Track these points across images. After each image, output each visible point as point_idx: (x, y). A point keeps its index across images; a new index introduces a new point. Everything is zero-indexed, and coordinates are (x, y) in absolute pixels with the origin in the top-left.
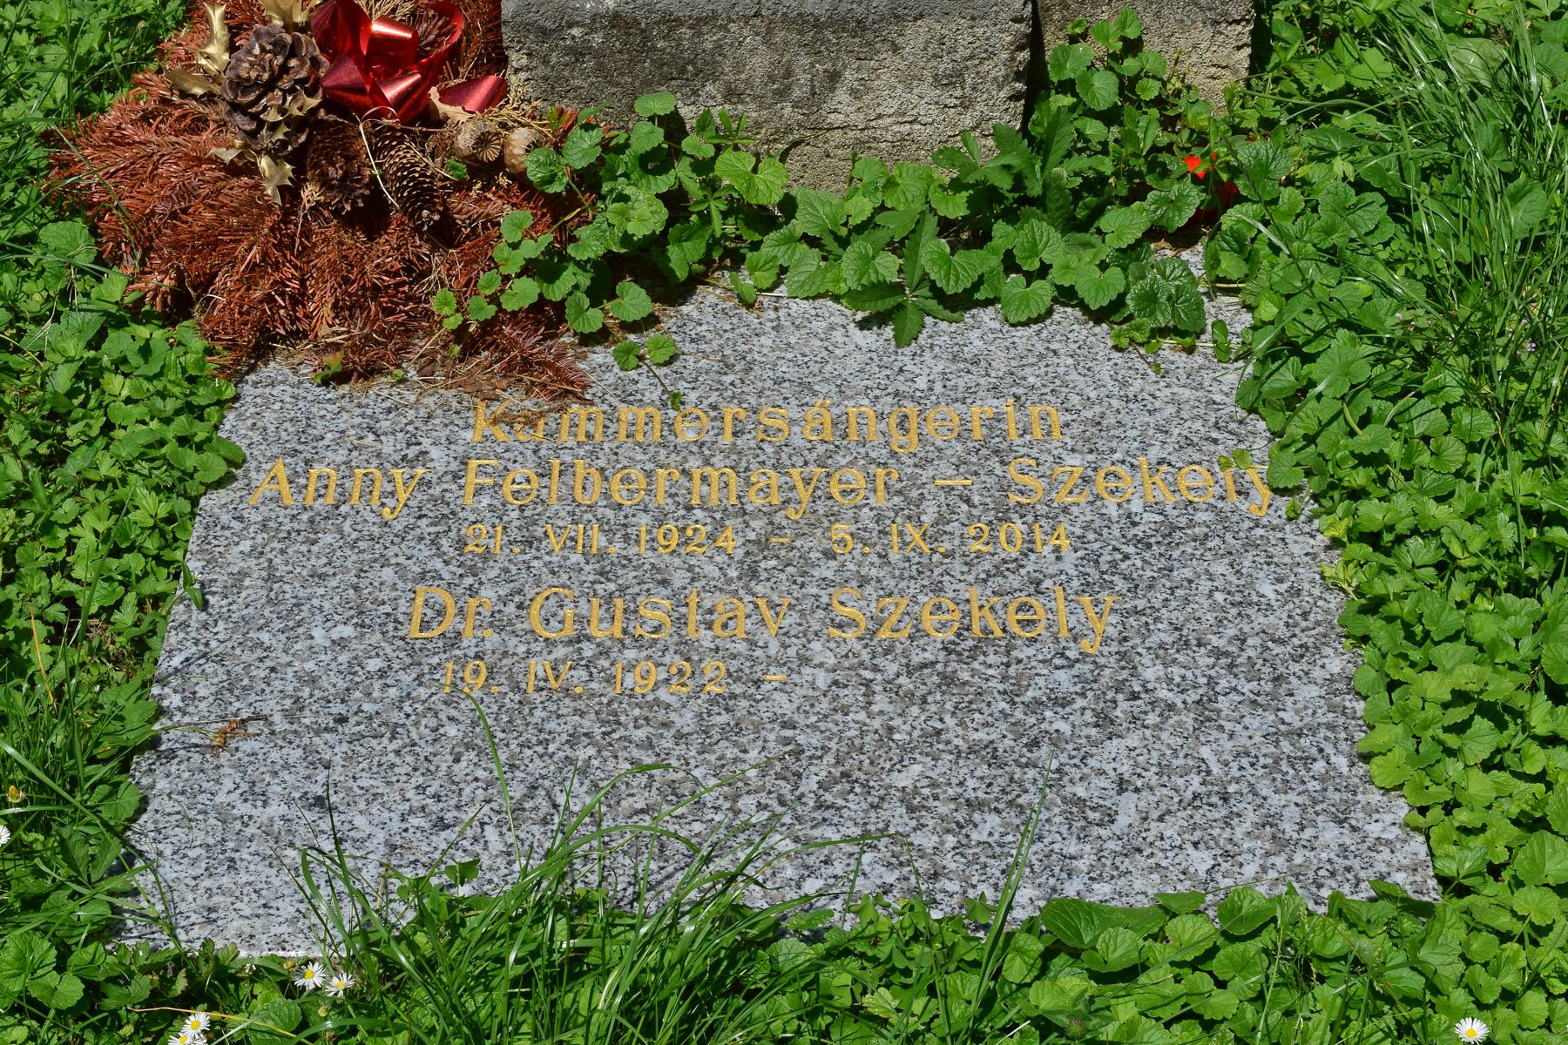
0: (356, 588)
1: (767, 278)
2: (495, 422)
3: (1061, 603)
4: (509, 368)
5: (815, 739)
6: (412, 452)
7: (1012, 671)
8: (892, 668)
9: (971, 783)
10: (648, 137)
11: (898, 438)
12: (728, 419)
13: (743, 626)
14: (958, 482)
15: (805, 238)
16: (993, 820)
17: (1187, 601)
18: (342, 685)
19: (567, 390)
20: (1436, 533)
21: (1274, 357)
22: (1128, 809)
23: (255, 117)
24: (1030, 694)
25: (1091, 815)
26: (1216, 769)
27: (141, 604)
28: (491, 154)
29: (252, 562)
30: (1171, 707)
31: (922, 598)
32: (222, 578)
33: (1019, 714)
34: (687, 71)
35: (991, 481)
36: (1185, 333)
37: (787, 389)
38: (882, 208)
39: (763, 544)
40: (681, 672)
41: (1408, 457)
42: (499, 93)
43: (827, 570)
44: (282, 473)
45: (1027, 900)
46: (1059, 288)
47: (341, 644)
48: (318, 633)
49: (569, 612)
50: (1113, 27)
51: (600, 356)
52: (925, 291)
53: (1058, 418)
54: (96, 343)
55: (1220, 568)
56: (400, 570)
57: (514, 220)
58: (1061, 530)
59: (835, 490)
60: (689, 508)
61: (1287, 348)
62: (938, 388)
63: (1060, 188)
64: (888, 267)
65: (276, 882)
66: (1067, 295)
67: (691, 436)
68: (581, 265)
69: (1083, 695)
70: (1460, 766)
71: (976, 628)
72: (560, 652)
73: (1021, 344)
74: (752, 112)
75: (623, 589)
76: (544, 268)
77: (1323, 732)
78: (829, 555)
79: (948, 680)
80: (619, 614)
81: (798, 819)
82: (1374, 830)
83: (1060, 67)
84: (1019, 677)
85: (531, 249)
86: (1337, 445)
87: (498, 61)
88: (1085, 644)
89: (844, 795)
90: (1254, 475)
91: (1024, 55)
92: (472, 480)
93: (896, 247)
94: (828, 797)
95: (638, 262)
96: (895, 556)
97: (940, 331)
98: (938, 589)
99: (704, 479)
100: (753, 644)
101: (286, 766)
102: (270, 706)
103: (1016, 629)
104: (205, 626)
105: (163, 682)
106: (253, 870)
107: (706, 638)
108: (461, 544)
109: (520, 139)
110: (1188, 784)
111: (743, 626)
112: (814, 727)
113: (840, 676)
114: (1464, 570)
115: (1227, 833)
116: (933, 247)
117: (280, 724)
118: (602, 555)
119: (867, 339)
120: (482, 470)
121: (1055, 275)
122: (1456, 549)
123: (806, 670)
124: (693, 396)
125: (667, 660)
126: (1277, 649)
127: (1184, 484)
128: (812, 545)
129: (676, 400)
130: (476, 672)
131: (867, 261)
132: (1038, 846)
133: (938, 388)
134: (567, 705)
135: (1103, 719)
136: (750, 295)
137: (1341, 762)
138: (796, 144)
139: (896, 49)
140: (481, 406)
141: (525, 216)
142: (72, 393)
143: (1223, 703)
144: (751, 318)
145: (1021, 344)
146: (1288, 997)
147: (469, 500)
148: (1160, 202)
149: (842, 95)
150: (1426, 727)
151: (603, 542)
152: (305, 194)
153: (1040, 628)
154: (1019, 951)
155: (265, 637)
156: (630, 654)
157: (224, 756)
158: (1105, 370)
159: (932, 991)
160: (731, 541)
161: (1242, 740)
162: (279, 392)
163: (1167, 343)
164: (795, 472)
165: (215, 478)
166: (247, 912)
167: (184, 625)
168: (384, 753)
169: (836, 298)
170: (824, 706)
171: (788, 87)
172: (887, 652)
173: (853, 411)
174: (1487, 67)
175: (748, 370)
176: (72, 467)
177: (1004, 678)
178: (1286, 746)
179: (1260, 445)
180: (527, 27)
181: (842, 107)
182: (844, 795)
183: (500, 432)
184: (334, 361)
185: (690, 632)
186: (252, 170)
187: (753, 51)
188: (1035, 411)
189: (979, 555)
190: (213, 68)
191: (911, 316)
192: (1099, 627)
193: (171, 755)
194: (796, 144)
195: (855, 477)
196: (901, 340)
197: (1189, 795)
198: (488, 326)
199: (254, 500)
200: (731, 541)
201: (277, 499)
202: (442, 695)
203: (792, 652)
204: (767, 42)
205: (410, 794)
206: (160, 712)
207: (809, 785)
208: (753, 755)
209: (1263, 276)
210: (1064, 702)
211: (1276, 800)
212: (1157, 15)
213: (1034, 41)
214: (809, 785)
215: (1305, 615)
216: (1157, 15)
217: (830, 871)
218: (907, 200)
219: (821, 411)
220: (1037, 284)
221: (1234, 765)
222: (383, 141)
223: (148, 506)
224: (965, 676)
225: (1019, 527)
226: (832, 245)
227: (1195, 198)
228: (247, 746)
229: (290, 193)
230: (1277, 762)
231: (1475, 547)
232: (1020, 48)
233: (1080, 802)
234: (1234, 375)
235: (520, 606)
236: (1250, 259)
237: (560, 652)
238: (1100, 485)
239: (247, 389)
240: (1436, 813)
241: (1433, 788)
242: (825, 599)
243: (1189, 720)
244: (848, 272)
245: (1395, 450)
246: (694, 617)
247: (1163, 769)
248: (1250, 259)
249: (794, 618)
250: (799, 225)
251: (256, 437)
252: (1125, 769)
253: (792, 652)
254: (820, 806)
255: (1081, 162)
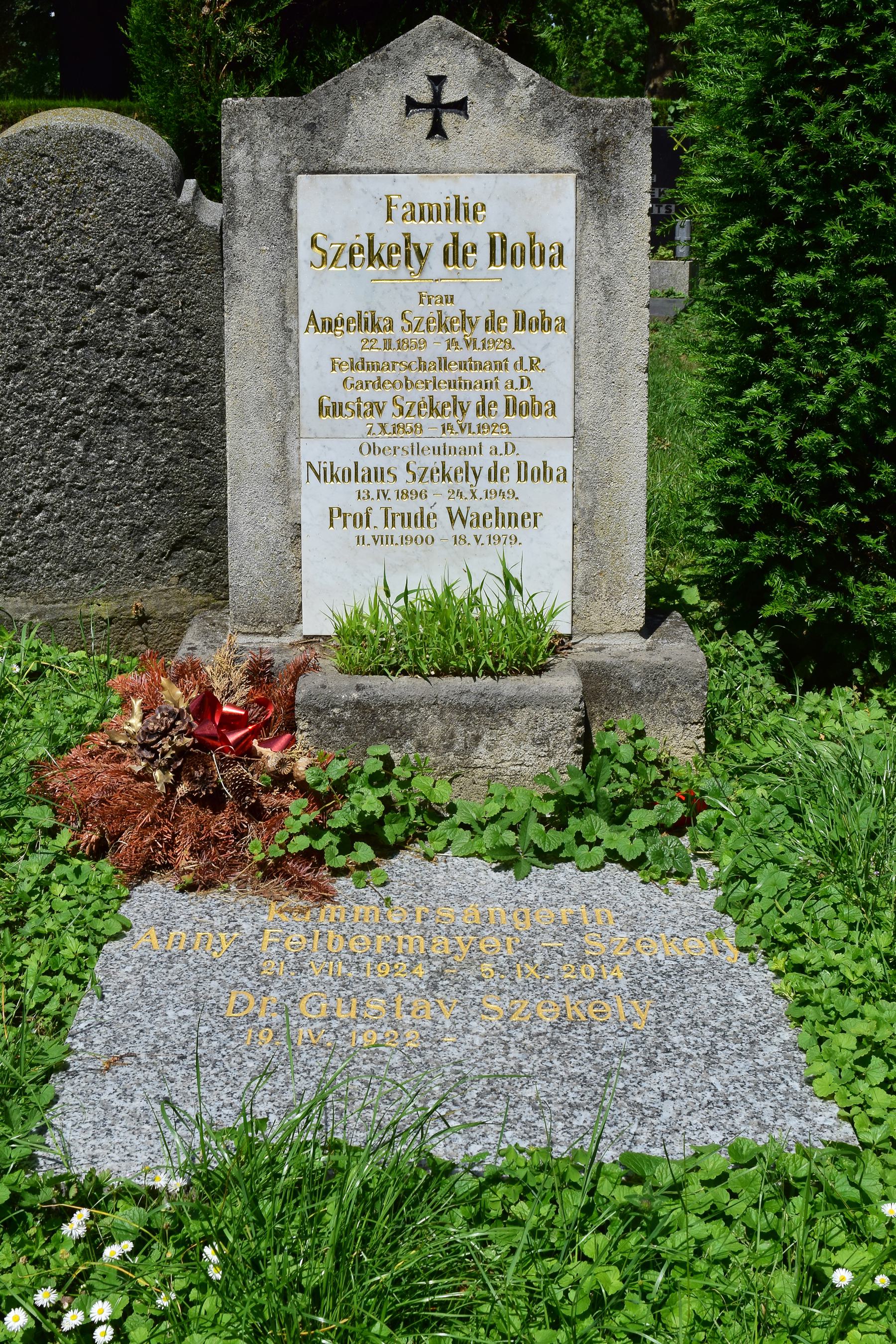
0: (195, 991)
1: (440, 846)
2: (281, 912)
3: (620, 1005)
4: (291, 884)
5: (475, 1072)
6: (231, 925)
7: (593, 1037)
8: (520, 1036)
9: (571, 1095)
10: (373, 766)
11: (518, 923)
12: (419, 913)
13: (429, 1013)
14: (555, 944)
15: (463, 826)
16: (586, 1115)
17: (694, 1003)
18: (183, 1039)
19: (325, 896)
20: (837, 968)
21: (733, 880)
22: (668, 1110)
23: (154, 751)
24: (604, 1049)
25: (646, 1112)
26: (720, 1089)
27: (62, 1001)
28: (286, 771)
29: (132, 977)
30: (690, 1056)
31: (537, 1001)
32: (113, 984)
33: (598, 1059)
34: (396, 733)
35: (574, 944)
36: (683, 876)
37: (452, 899)
38: (505, 810)
39: (441, 973)
40: (391, 1036)
41: (816, 931)
42: (293, 741)
43: (480, 986)
44: (153, 933)
45: (608, 1155)
46: (607, 850)
47: (185, 1018)
48: (171, 1014)
49: (323, 1005)
50: (628, 723)
51: (342, 881)
52: (531, 854)
53: (611, 915)
54: (50, 868)
55: (712, 987)
56: (222, 983)
57: (297, 804)
58: (617, 968)
59: (482, 947)
60: (396, 955)
61: (738, 875)
62: (541, 899)
63: (605, 798)
64: (510, 838)
65: (137, 1142)
66: (613, 856)
67: (397, 920)
68: (335, 831)
69: (636, 1050)
70: (867, 1085)
71: (570, 1015)
72: (318, 1025)
73: (588, 880)
74: (432, 757)
75: (356, 994)
76: (315, 830)
77: (782, 1070)
78: (480, 979)
79: (554, 1042)
80: (354, 1006)
81: (466, 1113)
82: (820, 1120)
83: (601, 742)
84: (597, 1041)
85: (307, 819)
86: (774, 922)
87: (291, 727)
88: (636, 1025)
89: (494, 1101)
90: (729, 943)
91: (581, 729)
92: (267, 939)
93: (513, 828)
94: (484, 1102)
95: (369, 830)
96: (519, 979)
97: (541, 874)
98: (546, 996)
99: (405, 941)
100: (435, 1022)
101: (147, 1081)
102: (139, 1049)
103: (594, 1017)
104: (102, 1008)
105: (73, 1036)
106: (121, 1135)
107: (407, 1019)
108: (259, 970)
109: (302, 763)
110: (704, 1096)
111: (429, 1013)
112: (474, 1066)
113: (489, 1039)
114: (855, 987)
115: (730, 1122)
116: (534, 830)
117: (144, 1058)
118: (344, 977)
119: (500, 876)
120: (272, 935)
121: (605, 844)
122: (849, 976)
123: (468, 1036)
124: (398, 901)
125: (383, 1029)
126: (751, 1028)
127: (687, 947)
128: (470, 974)
129: (388, 902)
130: (266, 1034)
131: (498, 835)
132: (615, 1128)
133: (541, 899)
134: (322, 1052)
135: (650, 1062)
136: (431, 854)
137: (796, 1086)
138: (457, 776)
139: (511, 724)
140: (273, 904)
141: (304, 802)
142: (32, 893)
143: (721, 1054)
144: (431, 865)
145: (588, 880)
146: (776, 1205)
147: (265, 949)
148: (662, 811)
149: (482, 749)
150: (844, 1063)
151: (345, 970)
152: (179, 790)
153: (608, 1016)
154: (607, 1175)
155: (138, 1014)
156: (361, 1027)
157: (108, 1075)
158: (637, 893)
159: (553, 1201)
160: (421, 971)
161: (734, 1073)
162: (156, 894)
163: (672, 881)
164: (459, 938)
165: (113, 933)
166: (117, 1158)
167: (89, 1008)
168: (208, 1074)
169: (480, 856)
170: (480, 1054)
171: (452, 744)
172: (516, 1027)
173: (491, 910)
174: (834, 754)
175: (430, 889)
176: (28, 929)
177: (588, 1041)
178: (761, 1077)
179: (730, 929)
180: (309, 707)
181: (482, 755)
182: (494, 1101)
183: (284, 917)
184: (187, 879)
185: (397, 1016)
186: (150, 778)
187: (433, 723)
188: (598, 911)
189: (569, 980)
190: (132, 730)
191: (524, 867)
192: (643, 1016)
193: (75, 1073)
194: (457, 776)
195: (495, 941)
196: (518, 877)
197: (705, 1102)
198: (279, 861)
199: (137, 945)
200: (421, 971)
201: (149, 947)
202: (245, 1046)
203: (459, 1027)
204: (441, 718)
205: (223, 1097)
206: (69, 1051)
207: (472, 1095)
208: (437, 1080)
209: (722, 847)
210: (625, 1053)
211: (758, 1105)
212: (653, 718)
213: (585, 722)
214: (472, 1095)
215: (765, 1011)
216: (653, 718)
217: (486, 1140)
218: (519, 805)
219: (473, 909)
220: (595, 849)
221: (731, 1087)
222: (225, 764)
223: (73, 946)
224: (565, 1040)
225: (592, 967)
226: (477, 828)
227: (681, 809)
228: (123, 1070)
229: (171, 788)
230: (757, 1085)
231: (860, 973)
232: (579, 725)
233: (639, 1105)
234: (711, 896)
235: (294, 1001)
236: (714, 838)
237: (318, 1025)
238: (639, 946)
239: (136, 894)
240: (855, 1110)
241: (852, 1098)
242: (478, 1001)
243: (702, 1063)
244: (487, 838)
245: (807, 926)
246: (399, 1008)
247: (687, 1088)
248: (714, 838)
249: (459, 1009)
250: (458, 818)
251: (139, 916)
252: (665, 1088)
253: (459, 1027)
254: (478, 1105)
255: (615, 785)
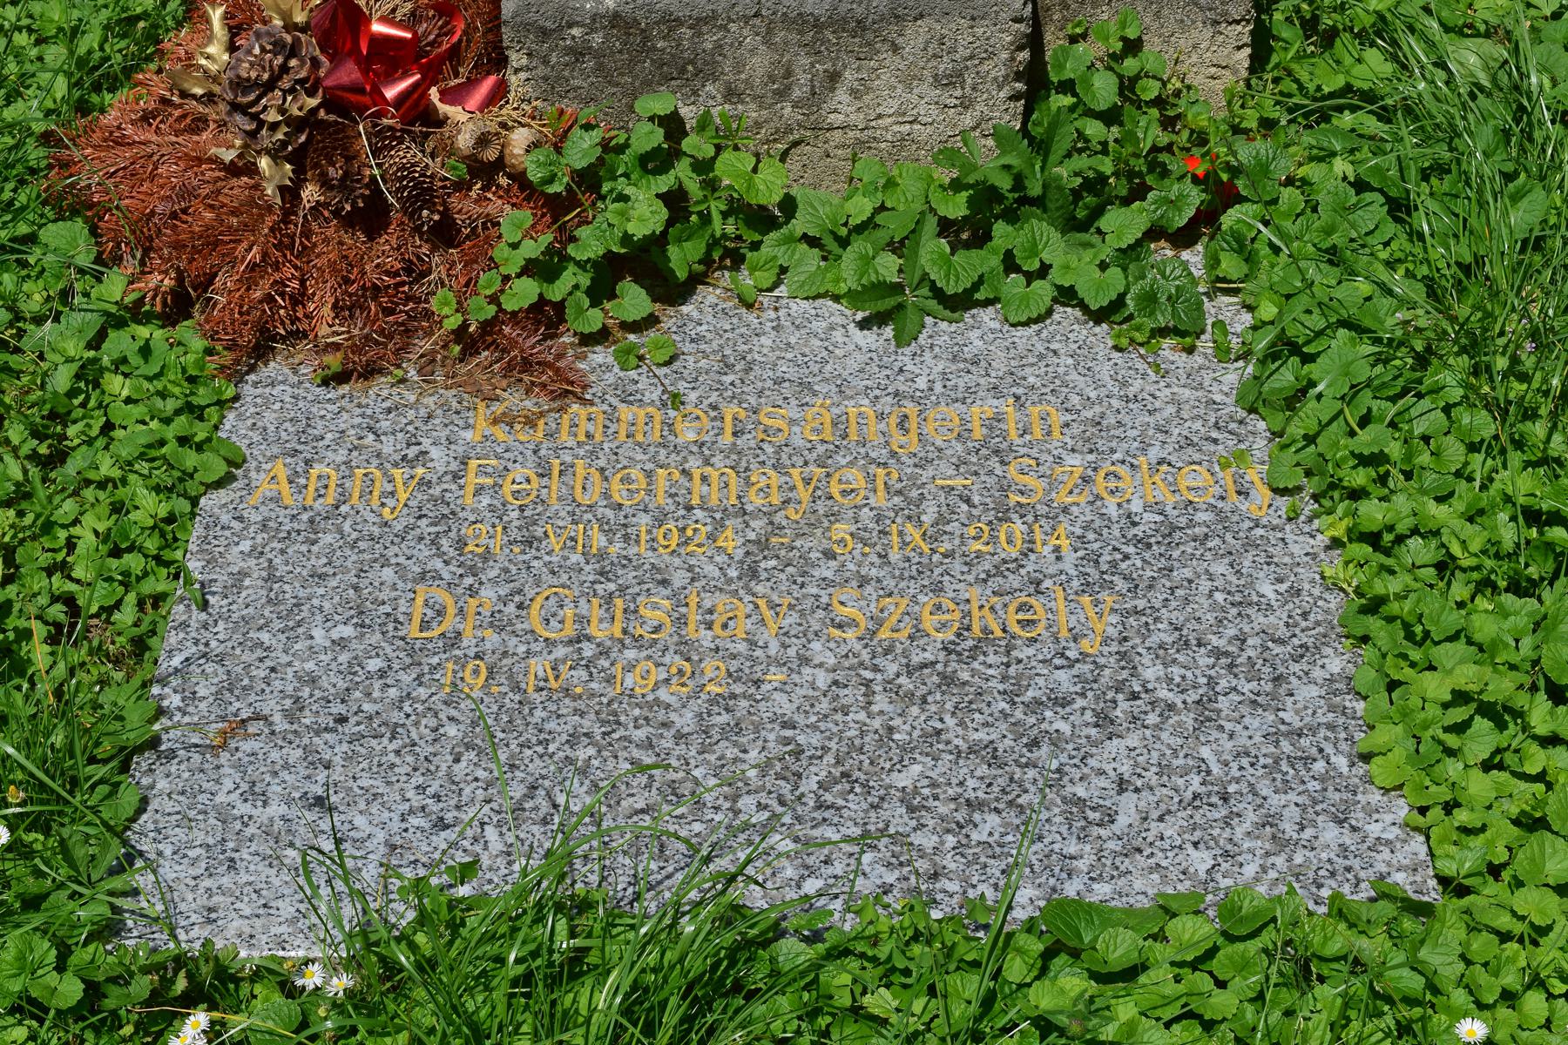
0: (356, 588)
1: (767, 278)
2: (495, 422)
3: (1061, 603)
4: (509, 368)
5: (815, 739)
6: (412, 452)
7: (1012, 671)
8: (892, 668)
9: (971, 783)
10: (648, 137)
11: (898, 438)
12: (728, 419)
13: (743, 626)
14: (958, 482)
15: (805, 238)
16: (993, 820)
17: (1187, 601)
18: (342, 685)
19: (567, 390)
20: (1436, 533)
21: (1274, 357)
22: (1128, 809)
23: (255, 117)
24: (1030, 694)
25: (1091, 815)
26: (1216, 769)
27: (141, 604)
28: (491, 154)
29: (252, 562)
30: (1171, 707)
31: (922, 598)
32: (222, 578)
33: (1019, 714)
34: (687, 71)
35: (991, 481)
36: (1185, 333)
37: (787, 389)
38: (882, 208)
39: (763, 544)
40: (681, 672)
41: (1408, 457)
42: (499, 93)
43: (827, 570)
44: (282, 473)
45: (1027, 900)
46: (1059, 288)
47: (341, 644)
48: (318, 633)
49: (569, 612)
50: (1113, 27)
51: (600, 356)
52: (925, 291)
53: (1058, 418)
54: (96, 343)
55: (1220, 568)
56: (400, 570)
57: (514, 220)
58: (1061, 530)
59: (835, 490)
60: (689, 508)
61: (1287, 348)
62: (938, 388)
63: (1060, 188)
64: (888, 267)
65: (276, 882)
66: (1067, 295)
67: (691, 436)
68: (581, 265)
69: (1083, 695)
70: (1460, 766)
71: (976, 628)
72: (560, 652)
73: (1021, 344)
74: (752, 112)
75: (623, 589)
76: (544, 268)
77: (1323, 732)
78: (829, 555)
79: (948, 680)
80: (619, 614)
81: (798, 819)
82: (1374, 830)
83: (1060, 67)
84: (1019, 677)
85: (531, 249)
86: (1337, 445)
87: (498, 61)
88: (1085, 644)
89: (844, 795)
90: (1254, 475)
91: (1024, 55)
92: (472, 480)
93: (896, 247)
94: (828, 797)
95: (638, 262)
96: (895, 556)
97: (940, 331)
98: (938, 589)
99: (704, 479)
100: (753, 644)
101: (286, 766)
102: (270, 706)
103: (1016, 629)
104: (205, 626)
105: (163, 682)
106: (253, 870)
107: (706, 638)
108: (461, 544)
109: (520, 139)
110: (1188, 784)
111: (743, 626)
112: (814, 727)
113: (840, 676)
114: (1464, 570)
115: (1227, 833)
116: (933, 247)
117: (280, 724)
118: (602, 555)
119: (867, 339)
120: (482, 470)
121: (1055, 275)
122: (1456, 549)
123: (806, 670)
124: (693, 396)
125: (667, 660)
126: (1277, 649)
127: (1184, 484)
128: (812, 545)
129: (676, 400)
130: (476, 672)
131: (867, 261)
132: (1038, 846)
133: (938, 388)
134: (567, 705)
135: (1103, 719)
136: (750, 295)
137: (1341, 762)
138: (796, 144)
139: (896, 49)
140: (481, 406)
141: (525, 216)
142: (72, 393)
143: (1223, 703)
144: (751, 318)
145: (1021, 344)
146: (1288, 997)
147: (469, 500)
148: (1160, 202)
149: (842, 95)
150: (1426, 727)
151: (603, 542)
152: (305, 194)
153: (1040, 628)
154: (1019, 951)
155: (265, 637)
156: (630, 654)
157: (224, 756)
158: (1105, 370)
159: (932, 991)
160: (731, 541)
161: (1242, 740)
162: (279, 392)
163: (1167, 343)
164: (795, 472)
165: (215, 478)
166: (247, 912)
167: (184, 625)
168: (384, 753)
169: (836, 298)
170: (824, 706)
171: (788, 87)
172: (887, 652)
173: (853, 411)
174: (1487, 67)
175: (748, 370)
176: (72, 467)
177: (1004, 678)
178: (1286, 746)
179: (1260, 445)
180: (527, 27)
181: (842, 107)
182: (844, 795)
183: (500, 432)
184: (334, 361)
185: (690, 632)
186: (252, 170)
187: (753, 51)
188: (1035, 411)
189: (979, 555)
190: (213, 68)
191: (911, 316)
192: (1099, 627)
193: (171, 755)
194: (796, 144)
195: (855, 477)
196: (901, 340)
197: (1189, 795)
198: (488, 326)
199: (254, 500)
200: (731, 541)
201: (277, 499)
202: (442, 695)
203: (792, 652)
204: (767, 42)
205: (410, 794)
206: (160, 712)
207: (809, 785)
208: (753, 755)
209: (1263, 276)
210: (1064, 702)
211: (1276, 800)
212: (1157, 15)
213: (1034, 41)
214: (809, 785)
215: (1305, 615)
216: (1157, 15)
217: (830, 871)
218: (907, 200)
219: (821, 411)
220: (1037, 284)
221: (1234, 765)
222: (383, 141)
223: (148, 506)
224: (965, 676)
225: (1019, 527)
226: (832, 245)
227: (1195, 198)
228: (247, 746)
229: (290, 193)
230: (1277, 762)
231: (1475, 547)
232: (1020, 48)
233: (1080, 802)
234: (1234, 375)
235: (520, 606)
236: (1250, 259)
237: (560, 652)
238: (1100, 485)
239: (247, 389)
240: (1436, 813)
241: (1433, 788)
242: (825, 599)
243: (1189, 720)
244: (848, 272)
245: (1395, 450)
246: (694, 617)
247: (1163, 769)
248: (1250, 259)
249: (794, 618)
250: (799, 225)
251: (256, 437)
252: (1125, 769)
253: (792, 652)
254: (820, 806)
255: (1081, 162)
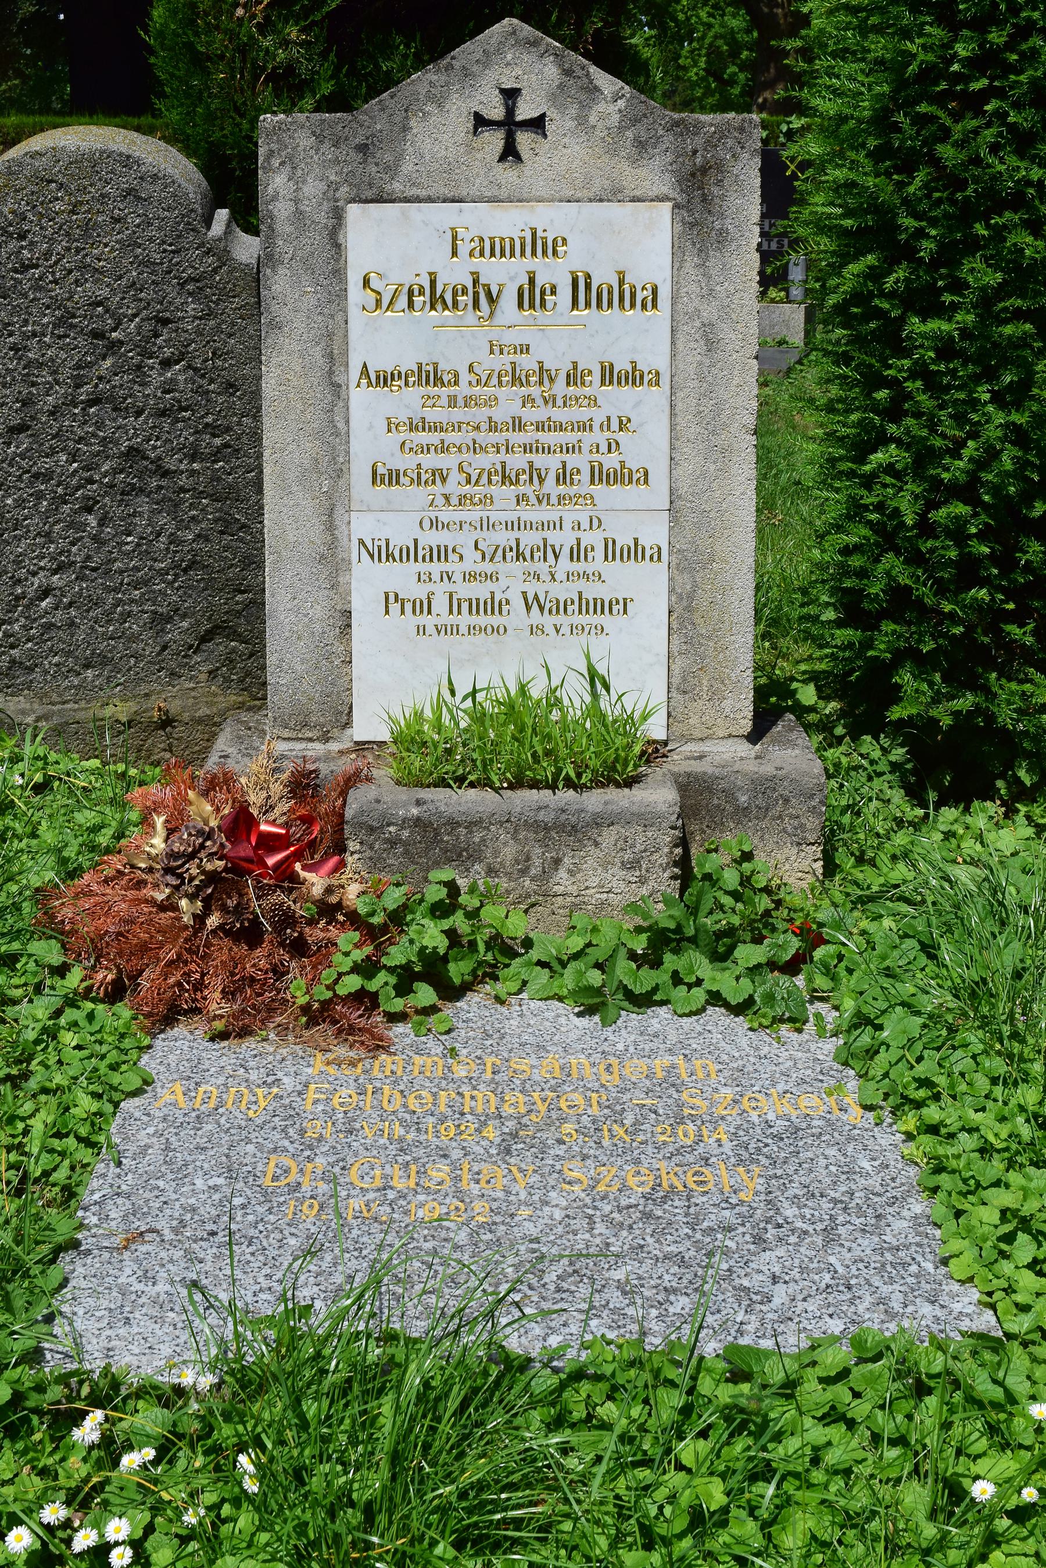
0: (227, 1156)
1: (514, 986)
2: (328, 1064)
3: (724, 1172)
4: (340, 1031)
5: (554, 1251)
6: (270, 1079)
7: (692, 1210)
8: (607, 1208)
9: (667, 1277)
10: (436, 893)
11: (605, 1077)
12: (489, 1065)
13: (501, 1182)
14: (648, 1102)
15: (540, 963)
16: (684, 1300)
17: (811, 1170)
18: (214, 1213)
19: (379, 1046)
20: (977, 1130)
21: (856, 1026)
22: (780, 1295)
23: (180, 876)
24: (706, 1224)
25: (755, 1297)
26: (841, 1270)
27: (73, 1168)
28: (333, 899)
29: (155, 1140)
30: (806, 1232)
31: (626, 1167)
32: (132, 1148)
33: (698, 1236)
34: (462, 856)
35: (670, 1101)
36: (797, 1022)
37: (528, 1049)
38: (589, 945)
39: (514, 1135)
40: (457, 1209)
41: (952, 1086)
42: (342, 864)
43: (560, 1150)
44: (179, 1088)
45: (710, 1347)
46: (709, 992)
47: (216, 1188)
48: (199, 1183)
49: (378, 1172)
50: (734, 843)
51: (400, 1028)
52: (620, 996)
53: (713, 1067)
54: (58, 1013)
55: (832, 1152)
56: (259, 1147)
57: (347, 938)
58: (720, 1129)
59: (563, 1105)
60: (462, 1114)
61: (862, 1021)
62: (632, 1049)
63: (706, 931)
64: (595, 978)
65: (160, 1333)
66: (715, 998)
67: (464, 1074)
68: (391, 970)
69: (743, 1225)
70: (1012, 1266)
71: (665, 1184)
72: (371, 1195)
73: (686, 1027)
74: (504, 884)
75: (416, 1160)
76: (367, 968)
77: (913, 1248)
78: (561, 1142)
79: (647, 1216)
80: (413, 1174)
81: (544, 1298)
82: (957, 1307)
83: (701, 865)
84: (697, 1214)
85: (358, 955)
86: (904, 1076)
87: (340, 848)
88: (742, 1195)
89: (576, 1284)
90: (850, 1100)
91: (679, 851)
92: (311, 1096)
93: (598, 966)
94: (565, 1285)
95: (431, 969)
96: (606, 1143)
97: (631, 1020)
98: (637, 1162)
99: (472, 1098)
100: (508, 1193)
101: (171, 1261)
102: (162, 1224)
103: (694, 1186)
104: (119, 1176)
105: (85, 1209)
106: (142, 1324)
107: (475, 1189)
108: (302, 1132)
109: (353, 890)
110: (822, 1279)
111: (501, 1182)
112: (554, 1243)
113: (570, 1212)
114: (998, 1151)
115: (853, 1309)
116: (623, 968)
117: (168, 1235)
118: (401, 1140)
119: (584, 1022)
120: (318, 1091)
121: (706, 985)
122: (991, 1138)
123: (546, 1209)
124: (465, 1052)
125: (447, 1201)
126: (876, 1199)
127: (802, 1105)
128: (549, 1136)
129: (453, 1052)
130: (311, 1206)
131: (581, 974)
132: (718, 1316)
133: (632, 1049)
134: (376, 1227)
135: (758, 1239)
136: (504, 996)
137: (929, 1266)
138: (533, 905)
139: (596, 844)
140: (319, 1055)
141: (355, 936)
142: (37, 1042)
143: (841, 1230)
144: (504, 1010)
145: (686, 1027)
146: (906, 1405)
147: (309, 1107)
148: (773, 946)
149: (562, 873)
150: (985, 1240)
151: (402, 1132)
152: (209, 922)
153: (710, 1186)
154: (709, 1371)
155: (161, 1183)
156: (421, 1198)
157: (126, 1255)
158: (744, 1042)
159: (646, 1402)
160: (491, 1133)
161: (857, 1252)
162: (182, 1043)
163: (784, 1027)
164: (536, 1095)
165: (132, 1088)
166: (137, 1351)
167: (104, 1176)
168: (243, 1253)
169: (561, 999)
170: (560, 1230)
171: (528, 868)
172: (603, 1199)
173: (574, 1061)
174: (973, 880)
175: (502, 1038)
176: (33, 1084)
177: (687, 1215)
178: (888, 1256)
179: (853, 1084)
180: (361, 825)
181: (562, 881)
182: (576, 1284)
183: (332, 1070)
184: (219, 1025)
185: (464, 1185)
186: (175, 908)
187: (505, 844)
188: (698, 1063)
189: (665, 1143)
190: (154, 852)
191: (612, 1011)
192: (751, 1185)
193: (88, 1252)
194: (533, 905)
195: (578, 1098)
196: (605, 1023)
197: (823, 1285)
198: (326, 1004)
199: (160, 1103)
200: (491, 1133)
201: (174, 1104)
202: (287, 1220)
203: (536, 1198)
204: (514, 838)
205: (261, 1280)
206: (81, 1226)
207: (551, 1277)
208: (511, 1260)
209: (843, 988)
210: (730, 1229)
211: (885, 1290)
212: (762, 838)
213: (683, 842)
214: (551, 1277)
215: (893, 1179)
216: (762, 838)
217: (567, 1330)
218: (606, 940)
219: (552, 1061)
220: (694, 990)
221: (854, 1268)
222: (262, 892)
223: (85, 1104)
224: (659, 1213)
225: (691, 1128)
226: (557, 967)
227: (795, 944)
228: (143, 1248)
229: (200, 919)
230: (883, 1265)
231: (1004, 1135)
232: (676, 846)
233: (747, 1290)
234: (830, 1046)
235: (343, 1168)
236: (834, 978)
237: (371, 1195)
238: (746, 1104)
239: (158, 1043)
240: (998, 1295)
241: (995, 1281)
242: (558, 1167)
243: (819, 1240)
244: (569, 978)
245: (942, 1081)
246: (466, 1176)
247: (802, 1270)
248: (834, 978)
249: (536, 1178)
250: (535, 955)
251: (162, 1069)
252: (777, 1269)
253: (536, 1198)
254: (558, 1290)
255: (718, 915)
